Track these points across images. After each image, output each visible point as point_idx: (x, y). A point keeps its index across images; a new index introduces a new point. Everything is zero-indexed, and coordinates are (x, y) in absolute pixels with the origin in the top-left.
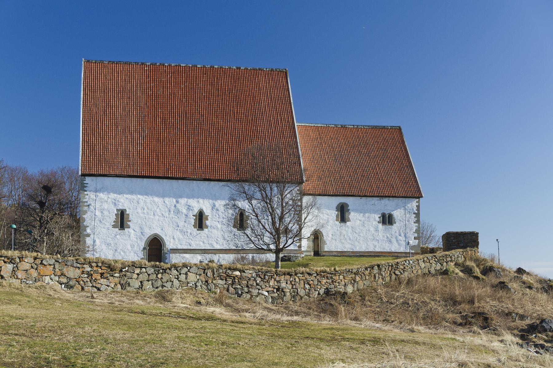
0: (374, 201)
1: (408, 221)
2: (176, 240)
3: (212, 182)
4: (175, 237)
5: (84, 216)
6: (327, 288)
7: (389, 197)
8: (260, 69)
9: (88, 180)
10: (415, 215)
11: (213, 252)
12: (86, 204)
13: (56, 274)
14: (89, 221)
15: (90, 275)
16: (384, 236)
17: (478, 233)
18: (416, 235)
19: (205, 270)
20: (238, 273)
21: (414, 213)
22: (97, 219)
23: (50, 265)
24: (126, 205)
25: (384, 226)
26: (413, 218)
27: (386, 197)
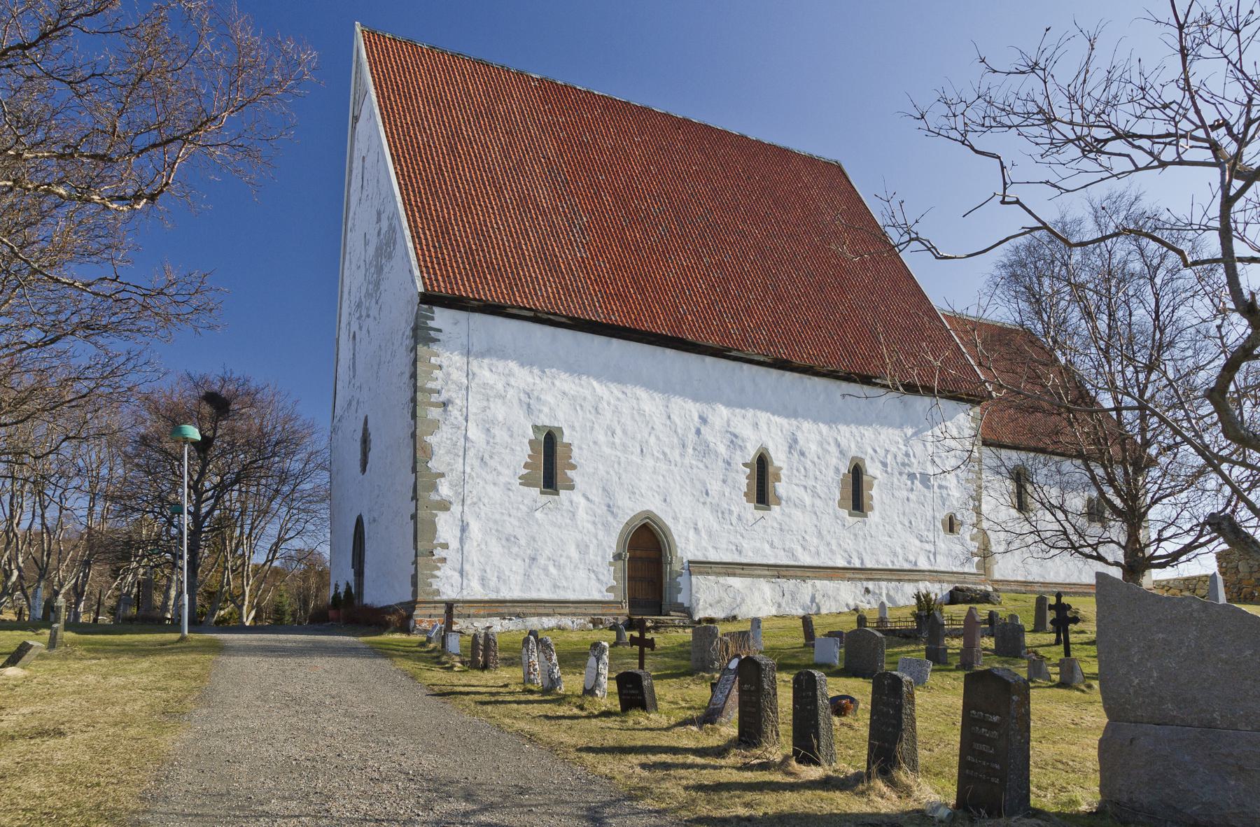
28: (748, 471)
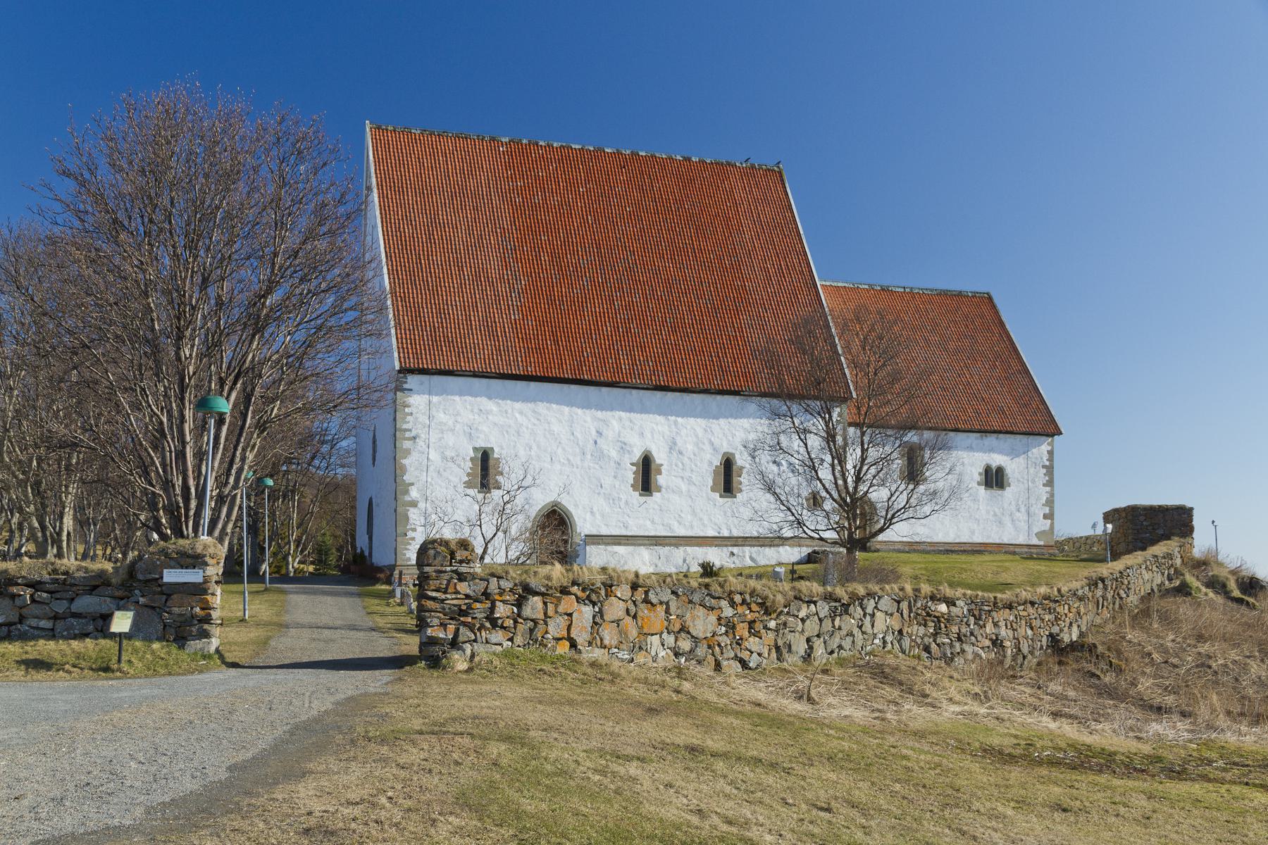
0: (969, 441)
1: (1033, 482)
2: (598, 516)
3: (670, 394)
4: (595, 509)
5: (404, 461)
6: (1051, 635)
7: (1000, 432)
8: (729, 164)
9: (413, 381)
11: (673, 541)
12: (407, 435)
13: (671, 627)
14: (416, 473)
15: (731, 627)
16: (988, 512)
17: (1192, 509)
18: (1047, 510)
20: (943, 608)
21: (1044, 467)
22: (431, 469)
23: (661, 603)
24: (493, 439)
25: (989, 492)
26: (1041, 477)
27: (995, 432)
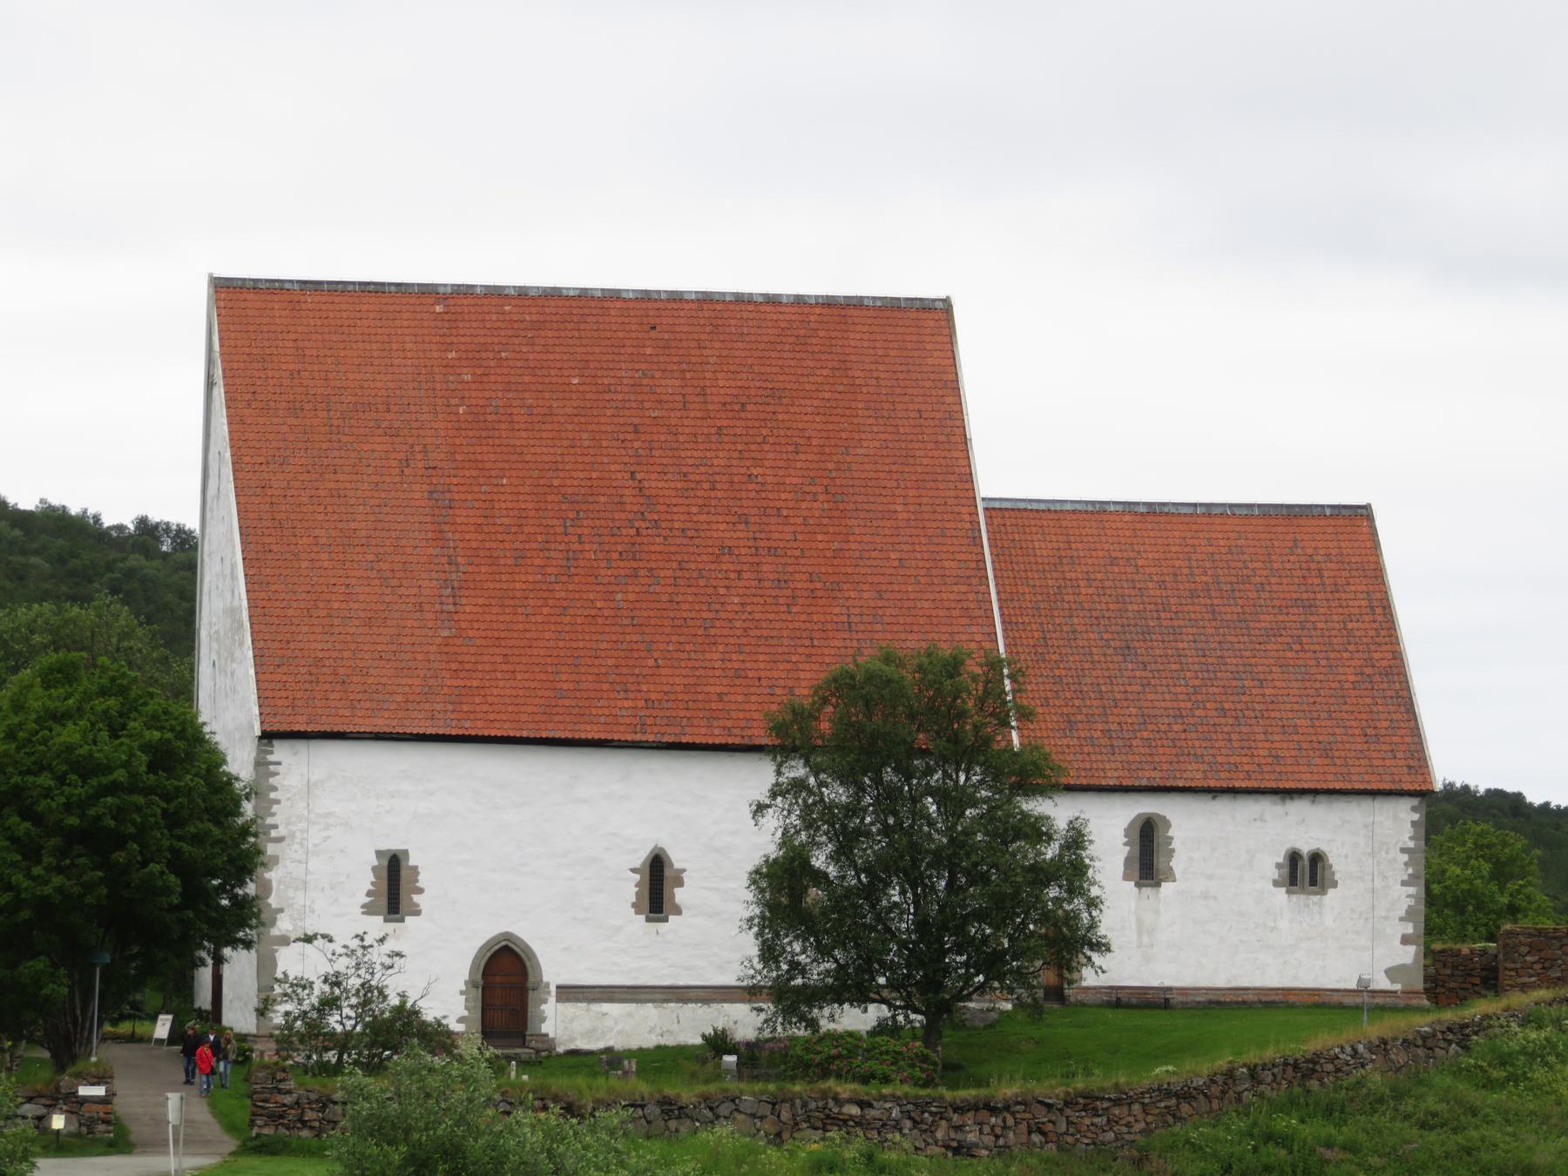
10: (1405, 857)
19: (774, 1104)
28: (637, 877)
